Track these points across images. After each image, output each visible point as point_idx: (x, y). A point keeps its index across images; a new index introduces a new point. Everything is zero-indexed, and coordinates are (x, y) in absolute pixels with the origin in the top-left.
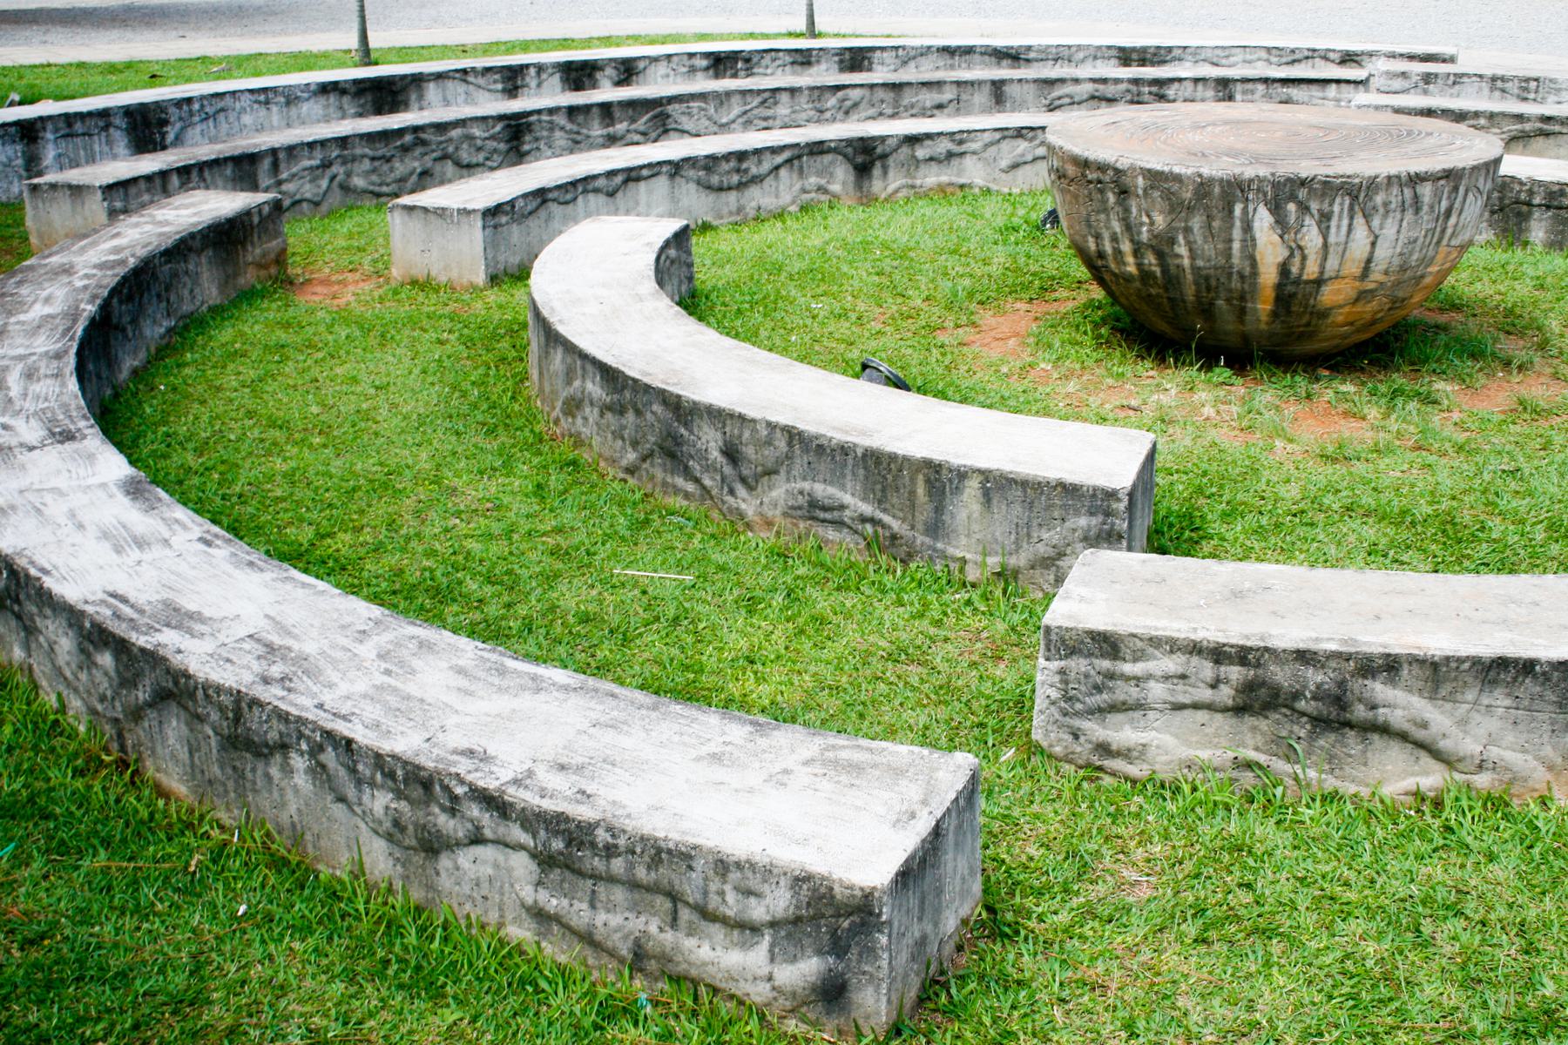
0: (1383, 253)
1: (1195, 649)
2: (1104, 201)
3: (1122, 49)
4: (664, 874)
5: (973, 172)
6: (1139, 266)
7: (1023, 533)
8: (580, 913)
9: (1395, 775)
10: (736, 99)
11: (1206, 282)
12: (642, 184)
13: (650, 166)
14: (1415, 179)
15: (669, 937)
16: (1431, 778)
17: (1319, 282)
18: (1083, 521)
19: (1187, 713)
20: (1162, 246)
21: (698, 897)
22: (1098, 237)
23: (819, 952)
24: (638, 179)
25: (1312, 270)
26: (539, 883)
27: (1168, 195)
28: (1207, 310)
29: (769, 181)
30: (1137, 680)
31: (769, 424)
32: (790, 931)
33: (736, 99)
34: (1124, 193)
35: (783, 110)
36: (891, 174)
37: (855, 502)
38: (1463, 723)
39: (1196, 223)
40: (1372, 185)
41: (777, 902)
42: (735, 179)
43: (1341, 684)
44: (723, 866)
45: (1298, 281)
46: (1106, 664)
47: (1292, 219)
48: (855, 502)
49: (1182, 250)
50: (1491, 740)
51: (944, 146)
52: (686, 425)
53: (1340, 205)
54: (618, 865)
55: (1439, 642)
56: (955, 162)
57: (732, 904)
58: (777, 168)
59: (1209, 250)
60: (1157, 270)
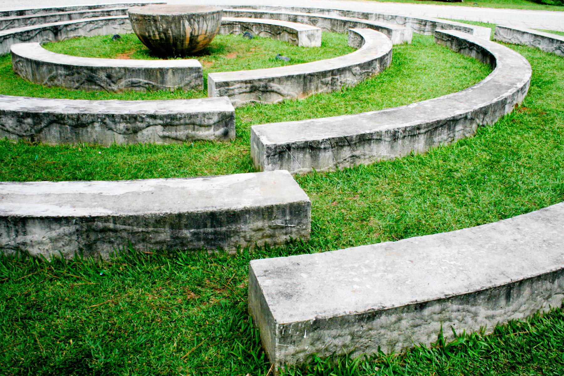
0: (209, 29)
1: (242, 82)
2: (150, 24)
3: (89, 7)
4: (192, 120)
5: (81, 32)
6: (160, 37)
7: (182, 79)
8: (173, 134)
9: (275, 99)
10: (4, 23)
11: (176, 39)
12: (7, 40)
13: (8, 35)
14: (213, 13)
15: (193, 132)
16: (280, 99)
17: (198, 36)
18: (194, 75)
19: (242, 94)
20: (165, 32)
21: (200, 123)
22: (149, 32)
23: (223, 127)
24: (6, 39)
25: (196, 34)
26: (164, 131)
27: (166, 20)
28: (175, 45)
29: (35, 38)
30: (233, 89)
31: (119, 68)
32: (217, 124)
33: (4, 23)
34: (155, 21)
35: (16, 25)
36: (63, 35)
37: (143, 80)
38: (284, 88)
39: (173, 25)
40: (206, 15)
41: (216, 119)
42: (27, 38)
43: (266, 84)
44: (204, 115)
45: (194, 36)
46: (227, 88)
47: (192, 23)
48: (143, 80)
49: (170, 32)
50: (289, 91)
51: (74, 27)
52: (95, 73)
53: (201, 19)
54: (182, 121)
55: (279, 75)
56: (77, 30)
57: (206, 122)
58: (36, 35)
59: (176, 31)
60: (164, 37)
